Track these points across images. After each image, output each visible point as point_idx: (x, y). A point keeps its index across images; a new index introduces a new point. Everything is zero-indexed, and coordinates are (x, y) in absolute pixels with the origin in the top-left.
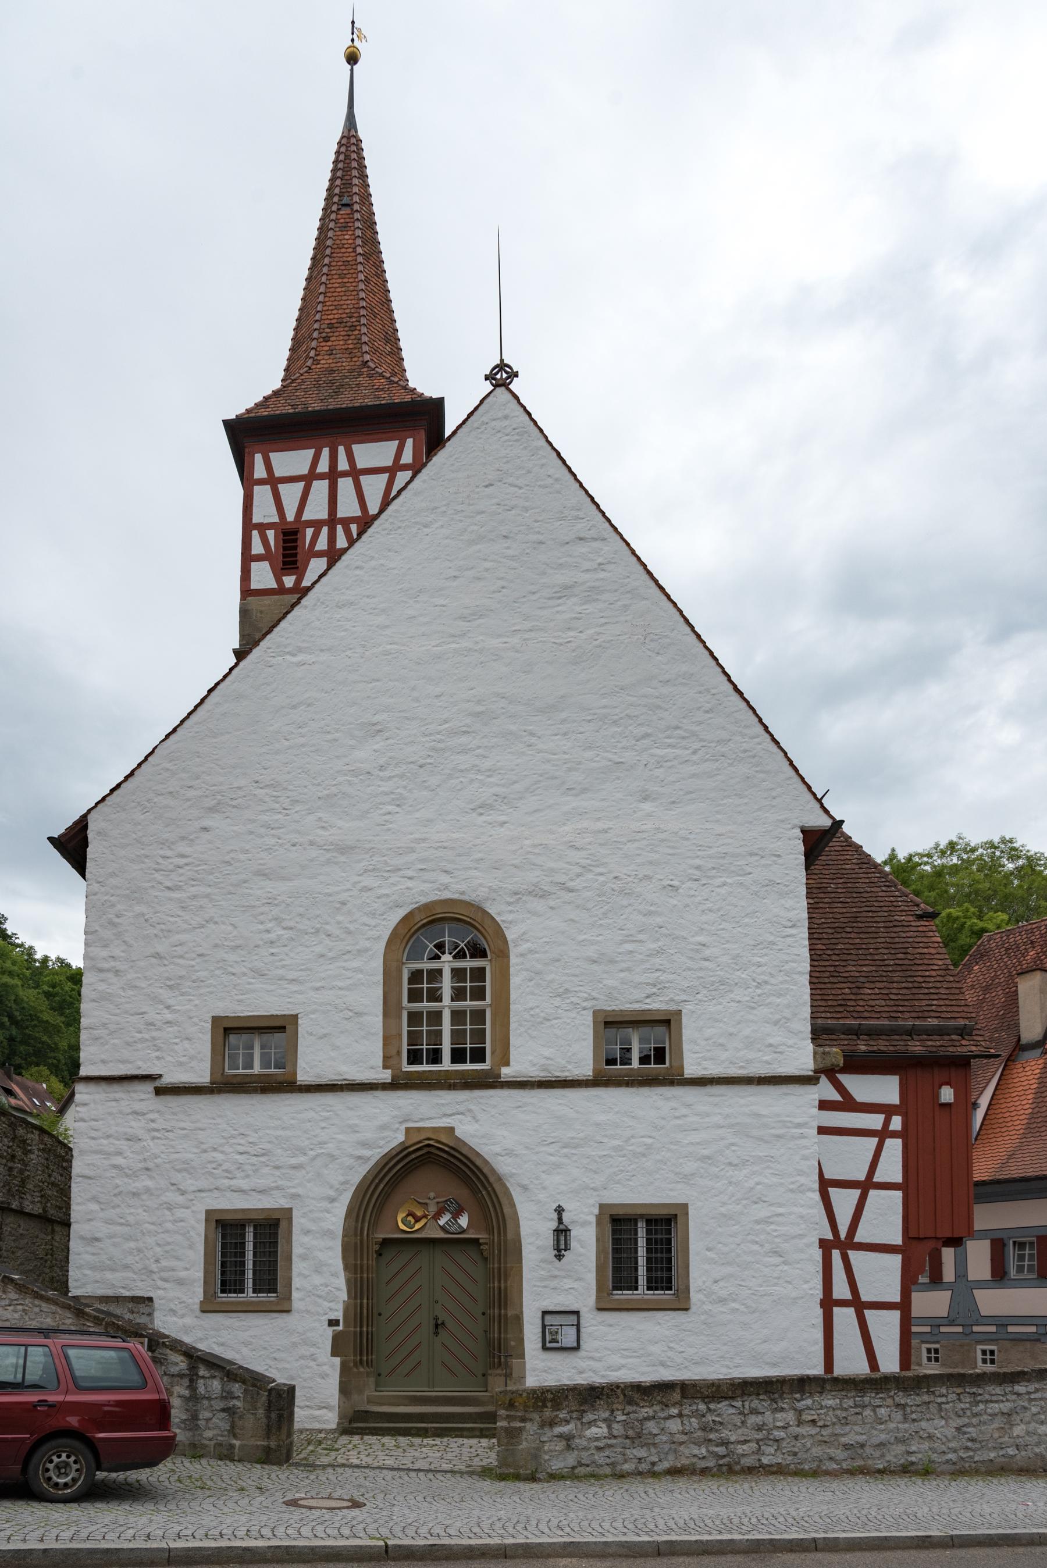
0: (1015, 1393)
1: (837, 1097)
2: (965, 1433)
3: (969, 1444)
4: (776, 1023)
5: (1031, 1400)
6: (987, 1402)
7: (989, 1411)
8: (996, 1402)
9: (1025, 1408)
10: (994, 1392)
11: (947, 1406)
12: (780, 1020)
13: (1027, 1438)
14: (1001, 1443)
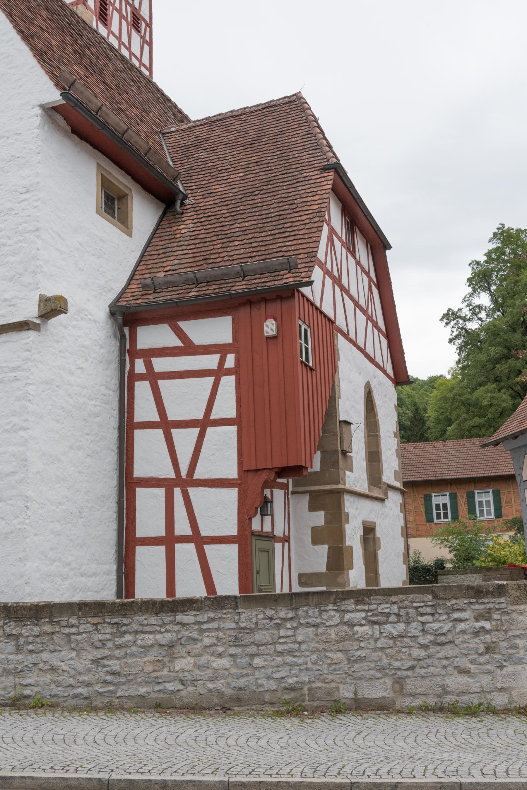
0: (178, 624)
1: (179, 343)
2: (105, 666)
3: (109, 678)
4: (11, 279)
5: (202, 631)
6: (136, 632)
7: (139, 642)
8: (150, 632)
9: (195, 640)
10: (146, 622)
11: (79, 637)
12: (14, 276)
13: (197, 672)
14: (157, 678)
